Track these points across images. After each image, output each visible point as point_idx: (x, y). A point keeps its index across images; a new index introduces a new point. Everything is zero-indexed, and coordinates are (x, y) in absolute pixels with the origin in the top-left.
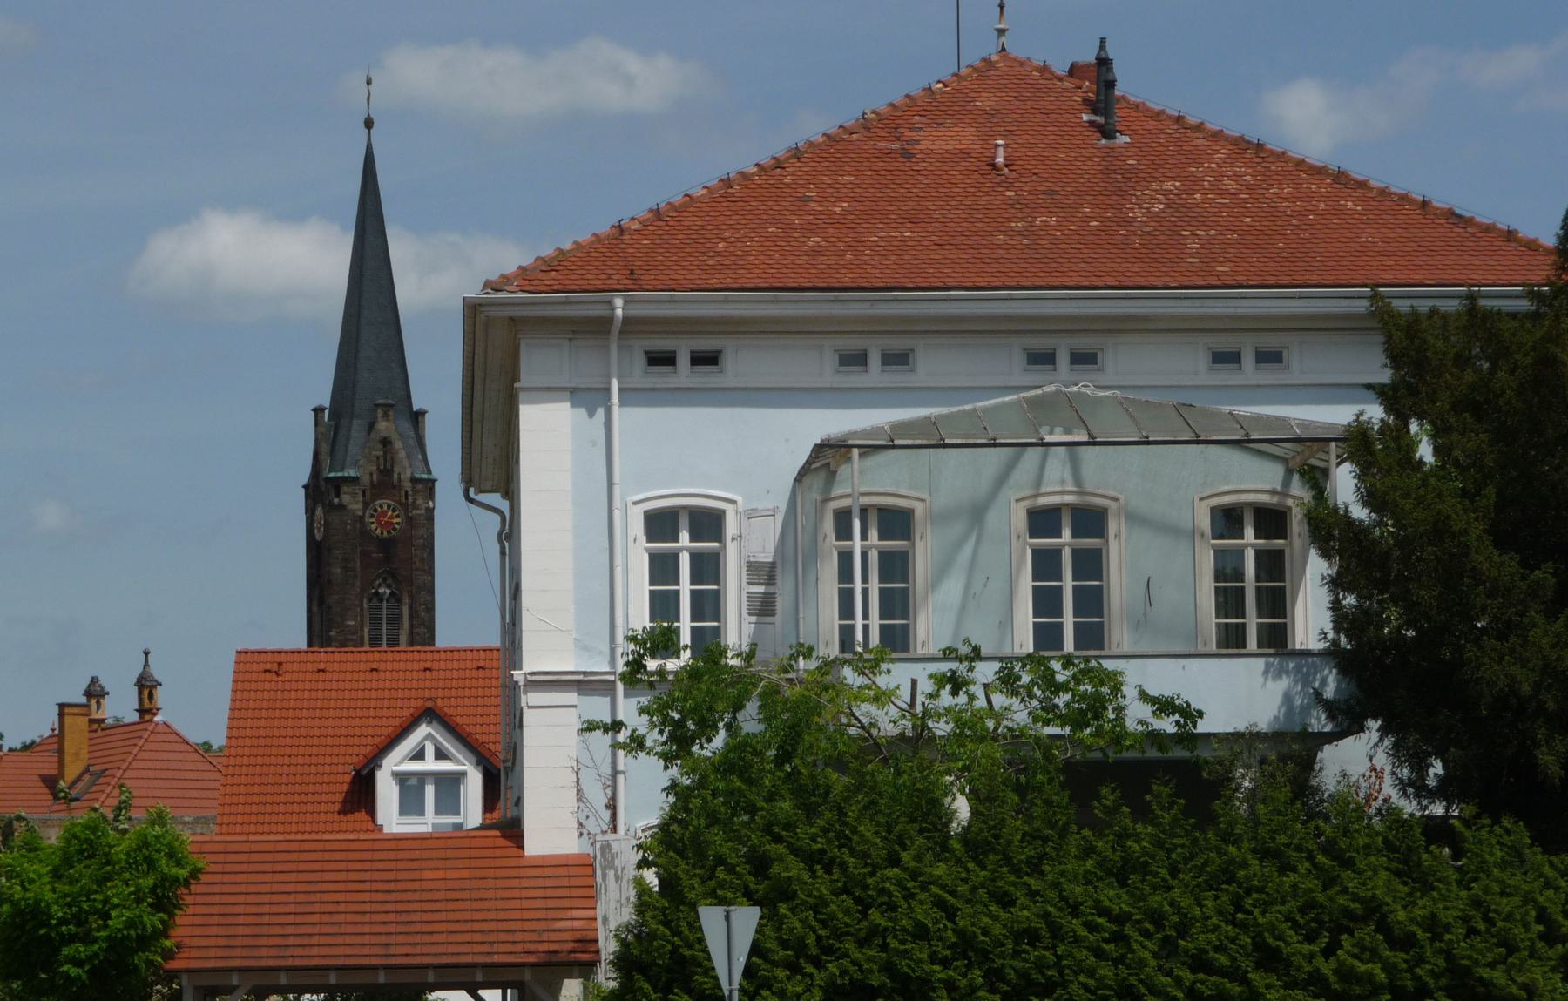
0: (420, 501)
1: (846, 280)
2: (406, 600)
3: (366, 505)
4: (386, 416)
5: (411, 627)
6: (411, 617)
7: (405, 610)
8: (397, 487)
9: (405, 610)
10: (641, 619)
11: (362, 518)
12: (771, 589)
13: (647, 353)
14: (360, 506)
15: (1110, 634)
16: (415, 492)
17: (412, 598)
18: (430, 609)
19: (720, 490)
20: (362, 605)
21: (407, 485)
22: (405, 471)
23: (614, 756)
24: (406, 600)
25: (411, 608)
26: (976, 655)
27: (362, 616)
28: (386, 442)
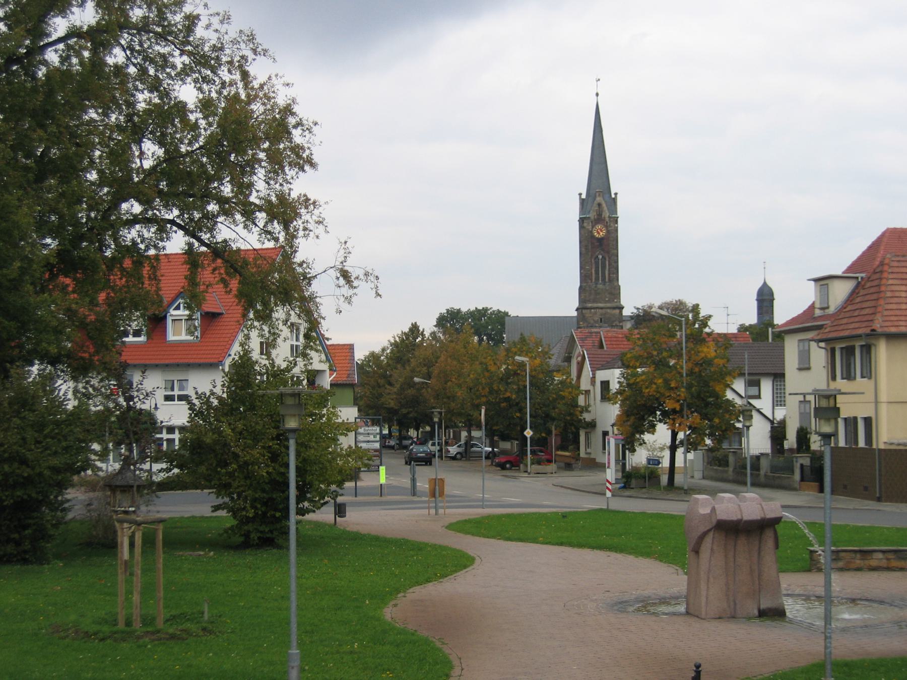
0: (612, 225)
1: (826, 298)
2: (607, 259)
3: (593, 227)
4: (599, 195)
5: (609, 269)
6: (609, 265)
7: (607, 262)
8: (604, 220)
9: (607, 262)
10: (591, 376)
11: (591, 232)
12: (863, 335)
13: (765, 284)
14: (590, 227)
15: (876, 365)
16: (610, 221)
17: (609, 258)
18: (617, 262)
19: (530, 405)
20: (591, 261)
21: (607, 219)
22: (606, 214)
23: (801, 394)
24: (607, 259)
25: (609, 261)
26: (304, 236)
27: (592, 265)
28: (599, 205)
